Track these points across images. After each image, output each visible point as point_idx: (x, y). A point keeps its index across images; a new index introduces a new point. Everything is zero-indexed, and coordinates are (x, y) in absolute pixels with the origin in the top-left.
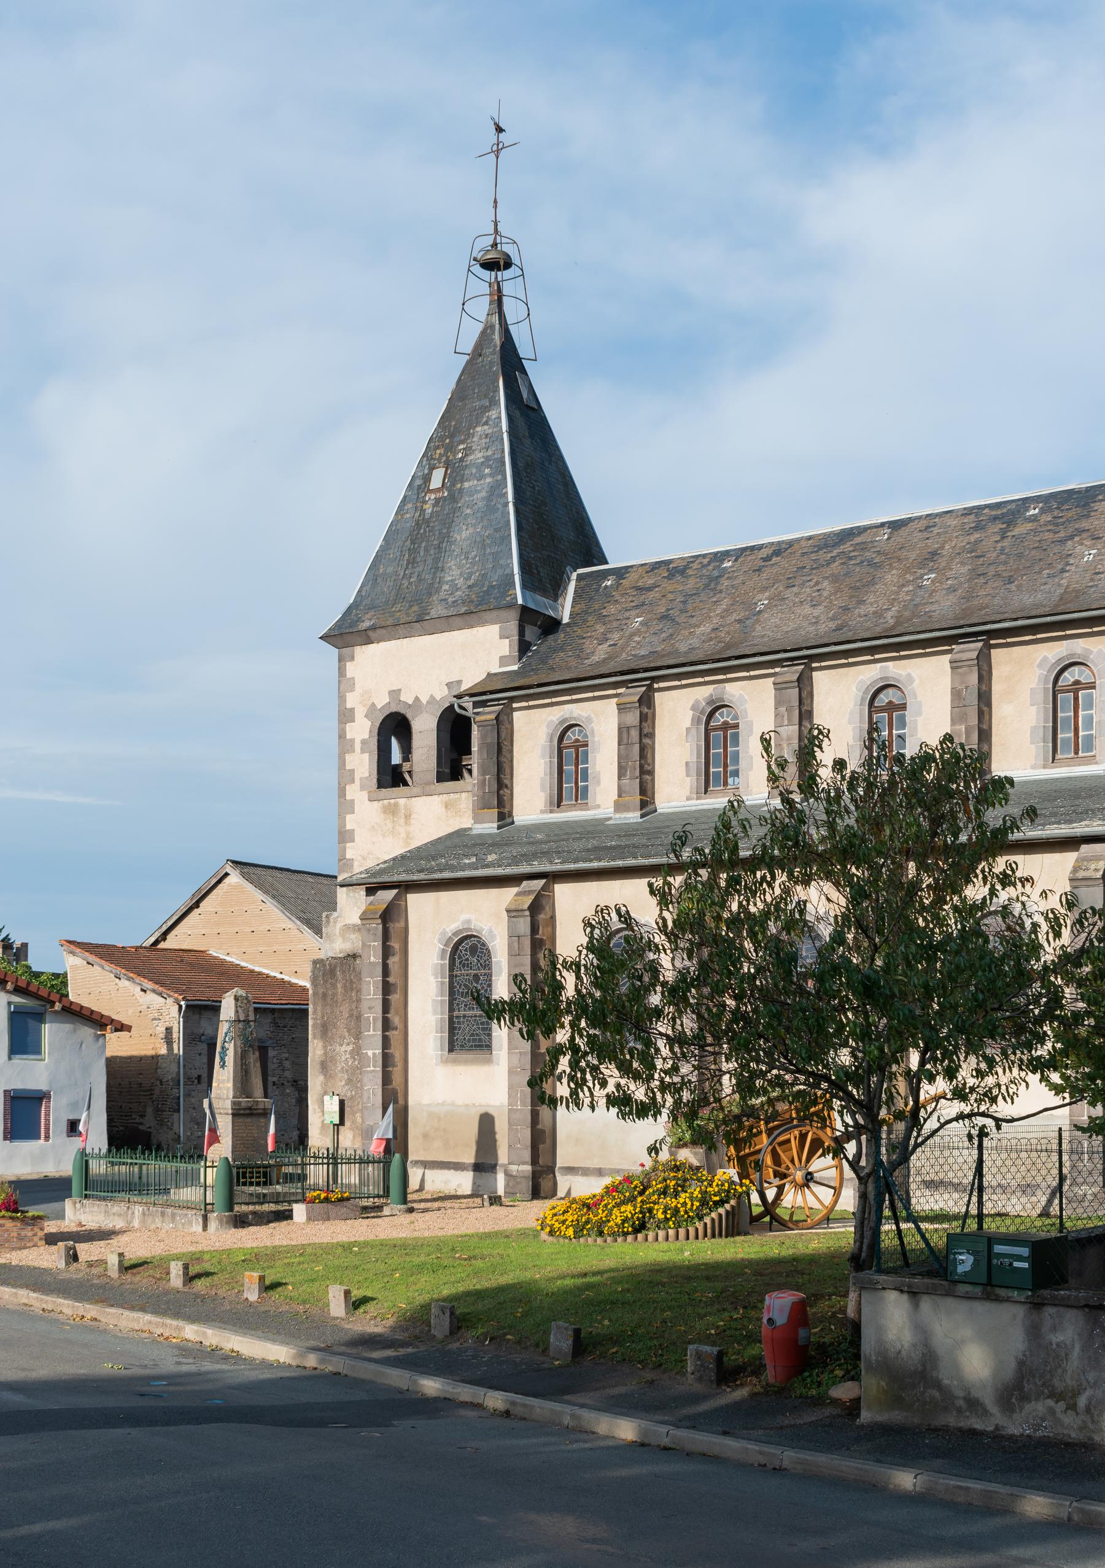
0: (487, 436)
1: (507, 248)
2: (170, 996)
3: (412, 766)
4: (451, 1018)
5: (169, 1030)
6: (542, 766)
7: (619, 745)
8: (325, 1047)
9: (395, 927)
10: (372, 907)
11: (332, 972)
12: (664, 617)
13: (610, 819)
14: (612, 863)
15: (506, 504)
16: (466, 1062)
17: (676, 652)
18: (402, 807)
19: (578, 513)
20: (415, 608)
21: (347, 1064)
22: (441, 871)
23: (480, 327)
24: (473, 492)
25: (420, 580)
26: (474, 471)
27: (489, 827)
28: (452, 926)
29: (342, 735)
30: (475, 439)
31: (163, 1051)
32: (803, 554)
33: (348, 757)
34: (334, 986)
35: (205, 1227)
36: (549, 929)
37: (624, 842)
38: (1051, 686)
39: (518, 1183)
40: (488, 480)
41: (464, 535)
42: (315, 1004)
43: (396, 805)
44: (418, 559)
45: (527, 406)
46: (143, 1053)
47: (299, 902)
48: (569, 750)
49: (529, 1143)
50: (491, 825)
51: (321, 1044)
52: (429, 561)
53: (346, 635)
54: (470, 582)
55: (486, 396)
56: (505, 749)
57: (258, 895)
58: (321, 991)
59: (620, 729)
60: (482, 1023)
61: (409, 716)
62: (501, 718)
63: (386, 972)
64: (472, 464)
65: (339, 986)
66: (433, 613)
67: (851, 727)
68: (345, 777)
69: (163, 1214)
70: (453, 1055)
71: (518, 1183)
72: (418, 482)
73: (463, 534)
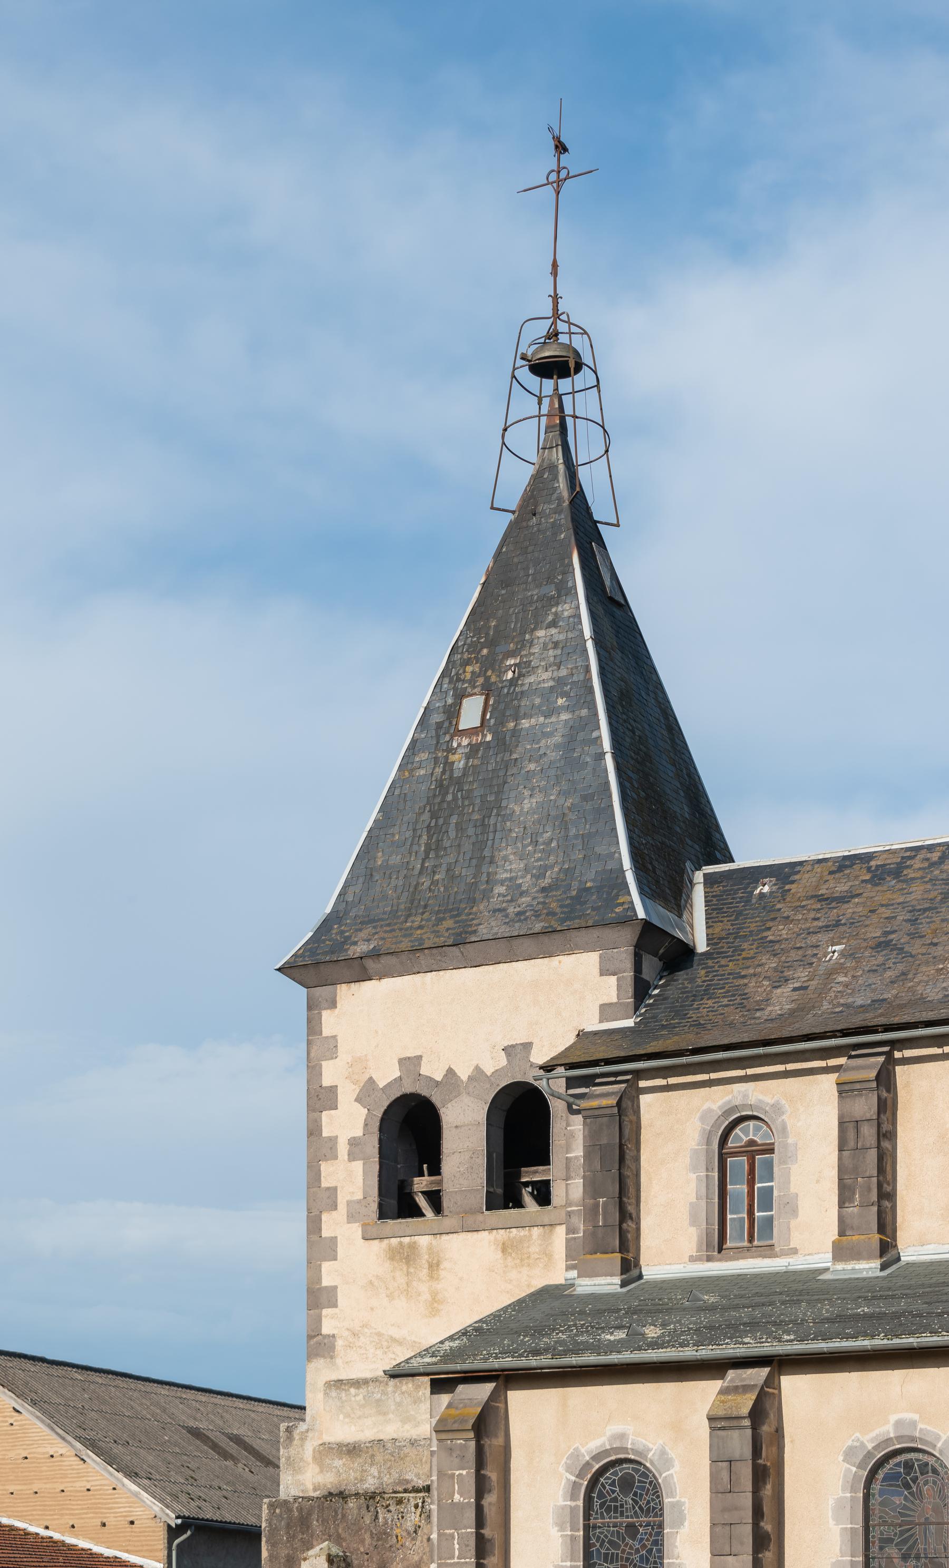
0: (556, 645)
1: (578, 343)
3: (440, 1183)
6: (693, 1185)
7: (841, 1150)
9: (493, 1443)
10: (453, 1411)
11: (304, 1522)
12: (882, 945)
13: (827, 1269)
15: (601, 756)
17: (922, 1001)
18: (424, 1251)
19: (689, 775)
20: (449, 923)
22: (576, 1352)
23: (530, 470)
25: (452, 876)
26: (537, 701)
27: (607, 1283)
28: (593, 1443)
29: (314, 1131)
30: (536, 649)
33: (325, 1167)
36: (774, 1449)
37: (881, 1307)
38: (715, 1146)
40: (564, 716)
41: (527, 805)
43: (413, 1247)
44: (446, 843)
45: (611, 599)
47: (71, 1410)
48: (740, 1162)
50: (609, 1280)
52: (467, 846)
53: (324, 964)
54: (547, 881)
55: (549, 580)
56: (629, 1155)
58: (283, 1552)
59: (842, 1124)
61: (436, 1100)
62: (624, 1105)
63: (480, 1522)
64: (534, 690)
67: (693, 1176)
68: (319, 1201)
72: (436, 718)
73: (525, 805)
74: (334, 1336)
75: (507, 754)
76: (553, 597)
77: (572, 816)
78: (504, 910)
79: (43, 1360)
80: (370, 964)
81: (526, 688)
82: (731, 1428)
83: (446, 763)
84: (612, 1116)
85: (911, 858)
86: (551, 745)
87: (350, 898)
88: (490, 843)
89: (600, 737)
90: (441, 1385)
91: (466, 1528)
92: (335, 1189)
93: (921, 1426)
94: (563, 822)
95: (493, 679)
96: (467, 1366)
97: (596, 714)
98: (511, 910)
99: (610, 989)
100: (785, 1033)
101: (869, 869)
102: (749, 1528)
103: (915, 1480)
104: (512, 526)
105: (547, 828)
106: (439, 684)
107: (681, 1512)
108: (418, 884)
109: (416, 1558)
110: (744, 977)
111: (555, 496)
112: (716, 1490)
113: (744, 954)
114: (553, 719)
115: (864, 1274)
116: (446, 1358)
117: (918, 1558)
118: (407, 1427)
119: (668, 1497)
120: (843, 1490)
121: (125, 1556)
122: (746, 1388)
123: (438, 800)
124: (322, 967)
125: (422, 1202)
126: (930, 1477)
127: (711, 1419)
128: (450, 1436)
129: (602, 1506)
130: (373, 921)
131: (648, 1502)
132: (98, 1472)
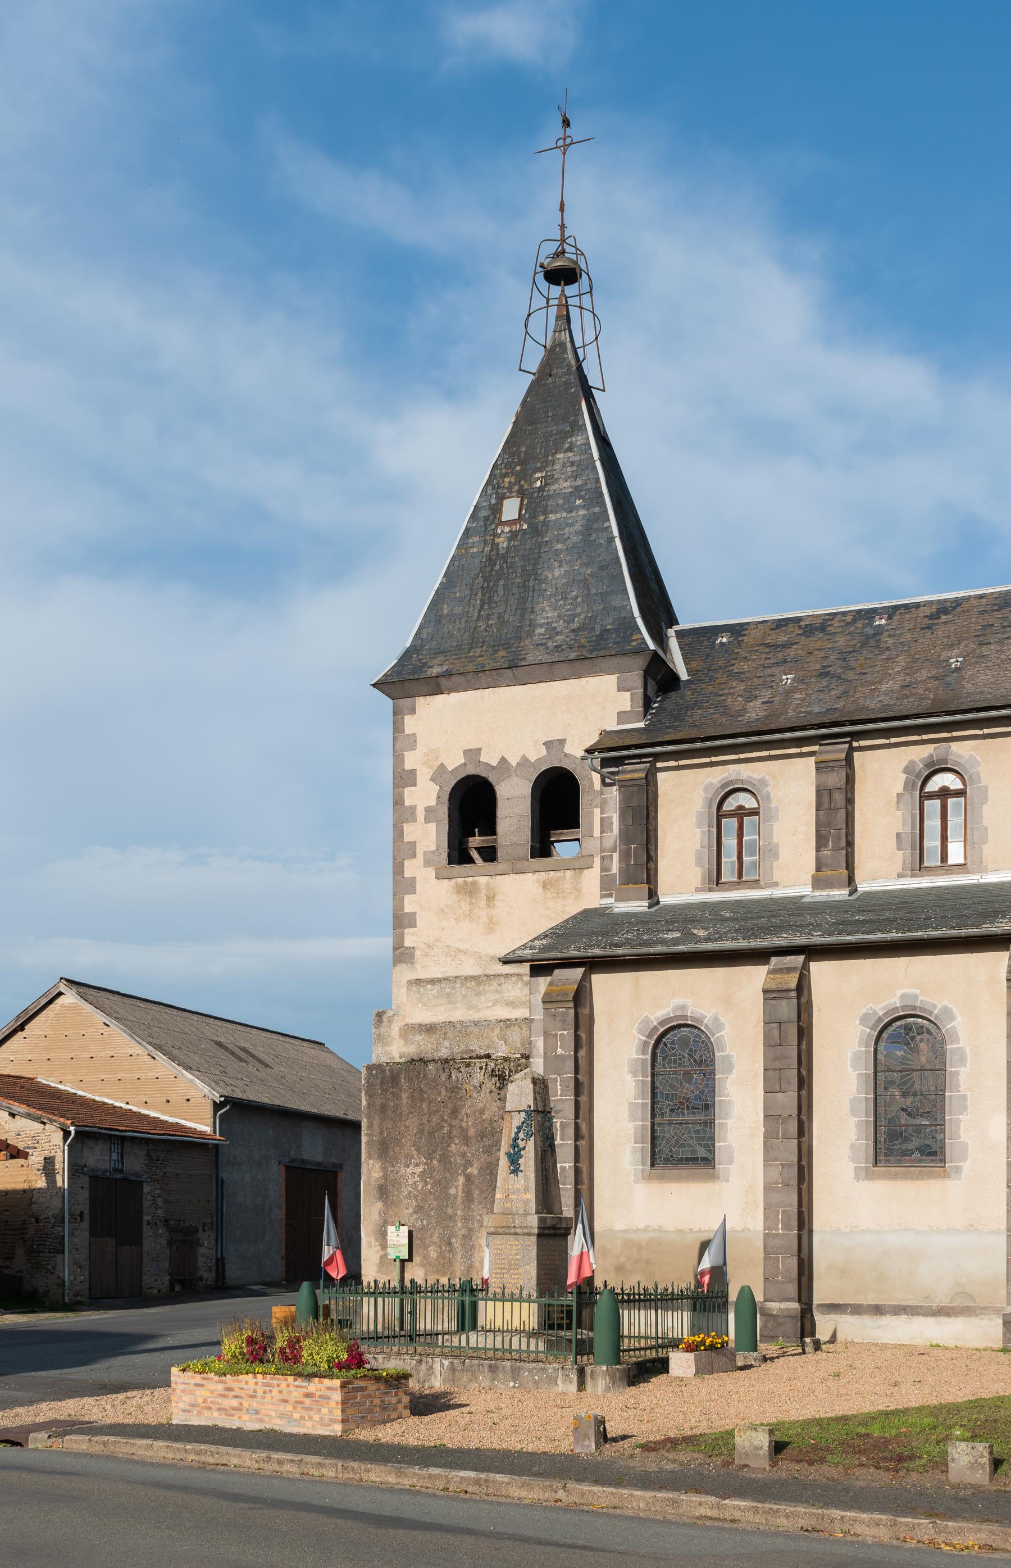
0: (572, 464)
2: (51, 1121)
3: (495, 840)
4: (653, 1125)
5: (49, 1162)
6: (698, 837)
8: (384, 1169)
9: (584, 1011)
10: (555, 988)
12: (823, 675)
14: (908, 934)
16: (679, 1179)
17: (865, 708)
21: (416, 1189)
24: (561, 525)
29: (398, 801)
30: (557, 467)
31: (41, 1183)
32: (982, 613)
33: (406, 827)
34: (397, 1096)
35: (581, 1385)
39: (780, 1324)
40: (582, 512)
41: (557, 574)
42: (369, 1117)
43: (474, 884)
44: (497, 599)
46: (9, 1187)
47: (143, 1027)
49: (795, 1274)
50: (639, 903)
51: (378, 1165)
52: (513, 601)
53: (407, 681)
54: (575, 625)
55: (565, 419)
56: (652, 814)
57: (100, 1017)
58: (378, 1102)
59: (818, 791)
60: (697, 1132)
61: (492, 780)
64: (556, 495)
65: (404, 1096)
66: (530, 658)
68: (402, 851)
69: (493, 1369)
70: (657, 1171)
71: (780, 1324)
72: (484, 513)
73: (556, 573)
74: (413, 948)
75: (540, 538)
76: (568, 432)
77: (591, 580)
78: (545, 644)
79: (118, 993)
80: (443, 682)
81: (551, 492)
82: (780, 998)
83: (493, 544)
84: (641, 785)
85: (829, 620)
86: (573, 533)
87: (424, 636)
88: (530, 599)
89: (610, 526)
90: (539, 969)
91: (567, 1073)
92: (415, 843)
93: (920, 998)
94: (585, 584)
95: (526, 487)
96: (565, 954)
97: (606, 511)
98: (550, 644)
99: (625, 701)
100: (773, 727)
101: (800, 627)
102: (795, 1071)
103: (913, 1038)
104: (533, 383)
105: (573, 589)
106: (484, 490)
107: (730, 1063)
108: (476, 627)
109: (481, 1105)
110: (721, 695)
111: (565, 364)
112: (768, 1044)
113: (718, 681)
114: (574, 514)
115: (837, 898)
116: (542, 949)
117: (915, 1095)
118: (471, 1012)
119: (719, 1051)
120: (860, 1046)
121: (183, 1122)
122: (789, 970)
123: (489, 569)
124: (406, 683)
125: (475, 854)
126: (925, 1036)
127: (765, 992)
128: (554, 1005)
129: (664, 1059)
130: (444, 652)
131: (701, 1056)
132: (164, 1066)
